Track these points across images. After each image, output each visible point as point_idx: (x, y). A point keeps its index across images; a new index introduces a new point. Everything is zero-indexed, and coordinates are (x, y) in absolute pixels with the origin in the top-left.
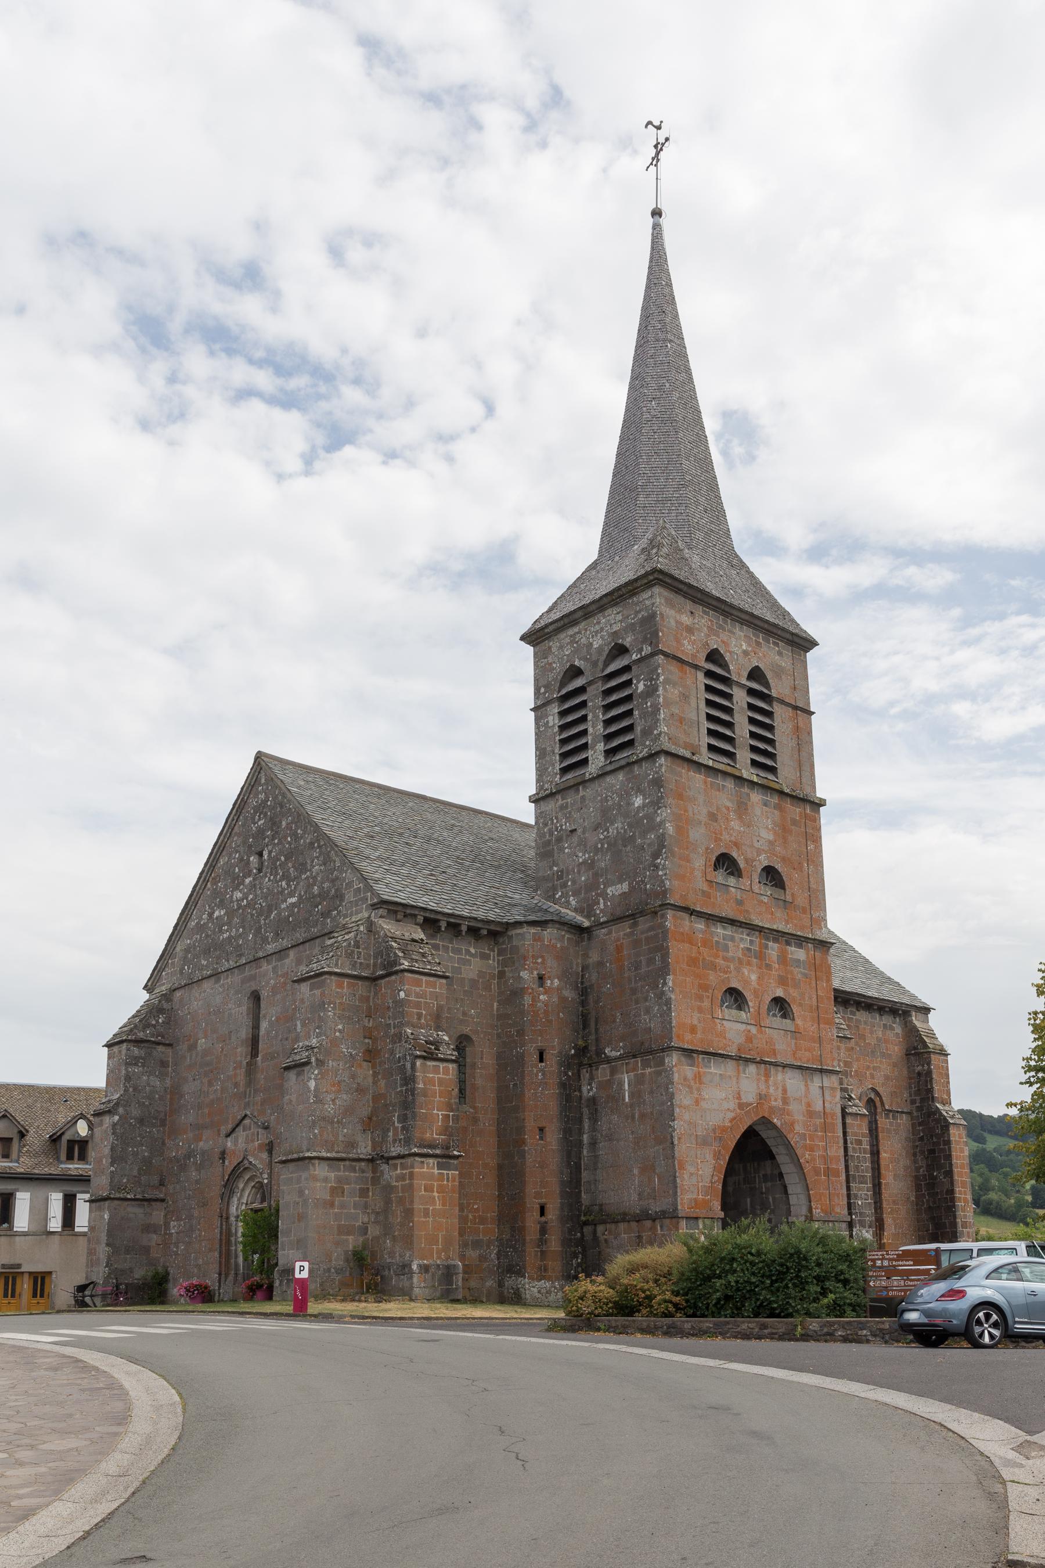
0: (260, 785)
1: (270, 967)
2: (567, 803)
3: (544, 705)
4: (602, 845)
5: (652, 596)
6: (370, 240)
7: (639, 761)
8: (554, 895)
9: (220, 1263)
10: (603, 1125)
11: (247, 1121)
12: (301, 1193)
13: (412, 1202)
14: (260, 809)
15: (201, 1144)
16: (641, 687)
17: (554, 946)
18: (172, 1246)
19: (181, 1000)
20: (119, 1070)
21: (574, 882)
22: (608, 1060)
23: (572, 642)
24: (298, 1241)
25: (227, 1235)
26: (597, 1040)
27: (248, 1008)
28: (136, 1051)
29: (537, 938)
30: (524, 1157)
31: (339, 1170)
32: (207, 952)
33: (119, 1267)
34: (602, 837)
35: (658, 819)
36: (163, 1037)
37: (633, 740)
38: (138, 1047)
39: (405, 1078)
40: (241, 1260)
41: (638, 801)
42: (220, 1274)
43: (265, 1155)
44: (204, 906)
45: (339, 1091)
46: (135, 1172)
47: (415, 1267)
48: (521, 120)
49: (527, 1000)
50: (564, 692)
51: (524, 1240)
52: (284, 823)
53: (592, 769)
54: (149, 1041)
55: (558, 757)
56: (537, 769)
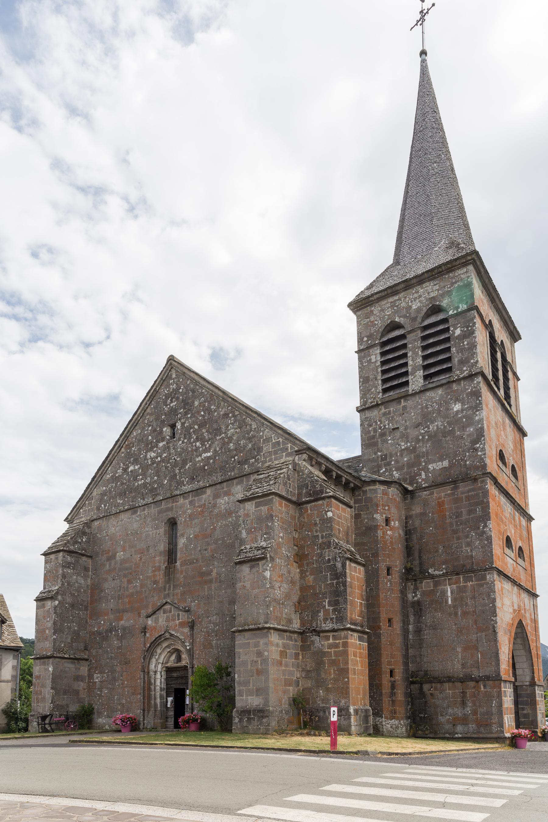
0: (171, 378)
1: (187, 501)
2: (390, 411)
3: (368, 348)
4: (423, 437)
5: (467, 272)
6: (50, 251)
7: (459, 380)
8: (379, 471)
9: (144, 703)
10: (427, 619)
11: (167, 607)
12: (259, 654)
13: (347, 663)
14: (172, 396)
15: (122, 622)
16: (458, 332)
17: (395, 500)
18: (96, 691)
19: (99, 528)
20: (57, 571)
21: (397, 461)
22: (432, 577)
23: (392, 307)
24: (257, 690)
25: (148, 686)
26: (421, 564)
27: (165, 530)
28: (69, 558)
29: (385, 493)
30: (380, 638)
31: (284, 639)
32: (122, 494)
33: (60, 703)
34: (423, 431)
35: (477, 418)
36: (86, 551)
37: (451, 367)
38: (70, 556)
39: (336, 574)
40: (158, 701)
41: (457, 407)
42: (144, 710)
43: (186, 630)
44: (119, 464)
45: (282, 581)
46: (69, 640)
47: (352, 711)
48: (126, 206)
49: (380, 533)
50: (385, 339)
51: (382, 693)
52: (196, 403)
53: (411, 388)
54: (76, 553)
55: (380, 382)
56: (361, 391)
